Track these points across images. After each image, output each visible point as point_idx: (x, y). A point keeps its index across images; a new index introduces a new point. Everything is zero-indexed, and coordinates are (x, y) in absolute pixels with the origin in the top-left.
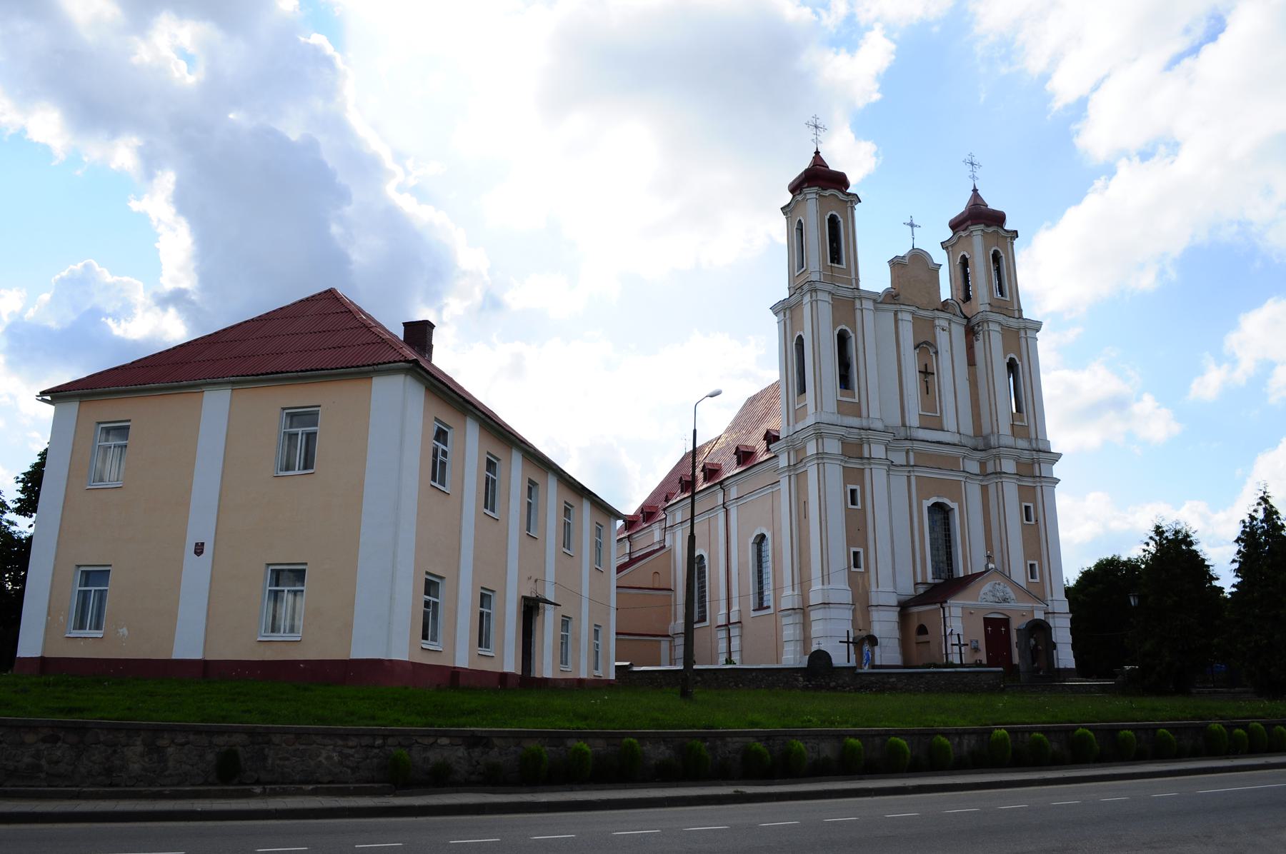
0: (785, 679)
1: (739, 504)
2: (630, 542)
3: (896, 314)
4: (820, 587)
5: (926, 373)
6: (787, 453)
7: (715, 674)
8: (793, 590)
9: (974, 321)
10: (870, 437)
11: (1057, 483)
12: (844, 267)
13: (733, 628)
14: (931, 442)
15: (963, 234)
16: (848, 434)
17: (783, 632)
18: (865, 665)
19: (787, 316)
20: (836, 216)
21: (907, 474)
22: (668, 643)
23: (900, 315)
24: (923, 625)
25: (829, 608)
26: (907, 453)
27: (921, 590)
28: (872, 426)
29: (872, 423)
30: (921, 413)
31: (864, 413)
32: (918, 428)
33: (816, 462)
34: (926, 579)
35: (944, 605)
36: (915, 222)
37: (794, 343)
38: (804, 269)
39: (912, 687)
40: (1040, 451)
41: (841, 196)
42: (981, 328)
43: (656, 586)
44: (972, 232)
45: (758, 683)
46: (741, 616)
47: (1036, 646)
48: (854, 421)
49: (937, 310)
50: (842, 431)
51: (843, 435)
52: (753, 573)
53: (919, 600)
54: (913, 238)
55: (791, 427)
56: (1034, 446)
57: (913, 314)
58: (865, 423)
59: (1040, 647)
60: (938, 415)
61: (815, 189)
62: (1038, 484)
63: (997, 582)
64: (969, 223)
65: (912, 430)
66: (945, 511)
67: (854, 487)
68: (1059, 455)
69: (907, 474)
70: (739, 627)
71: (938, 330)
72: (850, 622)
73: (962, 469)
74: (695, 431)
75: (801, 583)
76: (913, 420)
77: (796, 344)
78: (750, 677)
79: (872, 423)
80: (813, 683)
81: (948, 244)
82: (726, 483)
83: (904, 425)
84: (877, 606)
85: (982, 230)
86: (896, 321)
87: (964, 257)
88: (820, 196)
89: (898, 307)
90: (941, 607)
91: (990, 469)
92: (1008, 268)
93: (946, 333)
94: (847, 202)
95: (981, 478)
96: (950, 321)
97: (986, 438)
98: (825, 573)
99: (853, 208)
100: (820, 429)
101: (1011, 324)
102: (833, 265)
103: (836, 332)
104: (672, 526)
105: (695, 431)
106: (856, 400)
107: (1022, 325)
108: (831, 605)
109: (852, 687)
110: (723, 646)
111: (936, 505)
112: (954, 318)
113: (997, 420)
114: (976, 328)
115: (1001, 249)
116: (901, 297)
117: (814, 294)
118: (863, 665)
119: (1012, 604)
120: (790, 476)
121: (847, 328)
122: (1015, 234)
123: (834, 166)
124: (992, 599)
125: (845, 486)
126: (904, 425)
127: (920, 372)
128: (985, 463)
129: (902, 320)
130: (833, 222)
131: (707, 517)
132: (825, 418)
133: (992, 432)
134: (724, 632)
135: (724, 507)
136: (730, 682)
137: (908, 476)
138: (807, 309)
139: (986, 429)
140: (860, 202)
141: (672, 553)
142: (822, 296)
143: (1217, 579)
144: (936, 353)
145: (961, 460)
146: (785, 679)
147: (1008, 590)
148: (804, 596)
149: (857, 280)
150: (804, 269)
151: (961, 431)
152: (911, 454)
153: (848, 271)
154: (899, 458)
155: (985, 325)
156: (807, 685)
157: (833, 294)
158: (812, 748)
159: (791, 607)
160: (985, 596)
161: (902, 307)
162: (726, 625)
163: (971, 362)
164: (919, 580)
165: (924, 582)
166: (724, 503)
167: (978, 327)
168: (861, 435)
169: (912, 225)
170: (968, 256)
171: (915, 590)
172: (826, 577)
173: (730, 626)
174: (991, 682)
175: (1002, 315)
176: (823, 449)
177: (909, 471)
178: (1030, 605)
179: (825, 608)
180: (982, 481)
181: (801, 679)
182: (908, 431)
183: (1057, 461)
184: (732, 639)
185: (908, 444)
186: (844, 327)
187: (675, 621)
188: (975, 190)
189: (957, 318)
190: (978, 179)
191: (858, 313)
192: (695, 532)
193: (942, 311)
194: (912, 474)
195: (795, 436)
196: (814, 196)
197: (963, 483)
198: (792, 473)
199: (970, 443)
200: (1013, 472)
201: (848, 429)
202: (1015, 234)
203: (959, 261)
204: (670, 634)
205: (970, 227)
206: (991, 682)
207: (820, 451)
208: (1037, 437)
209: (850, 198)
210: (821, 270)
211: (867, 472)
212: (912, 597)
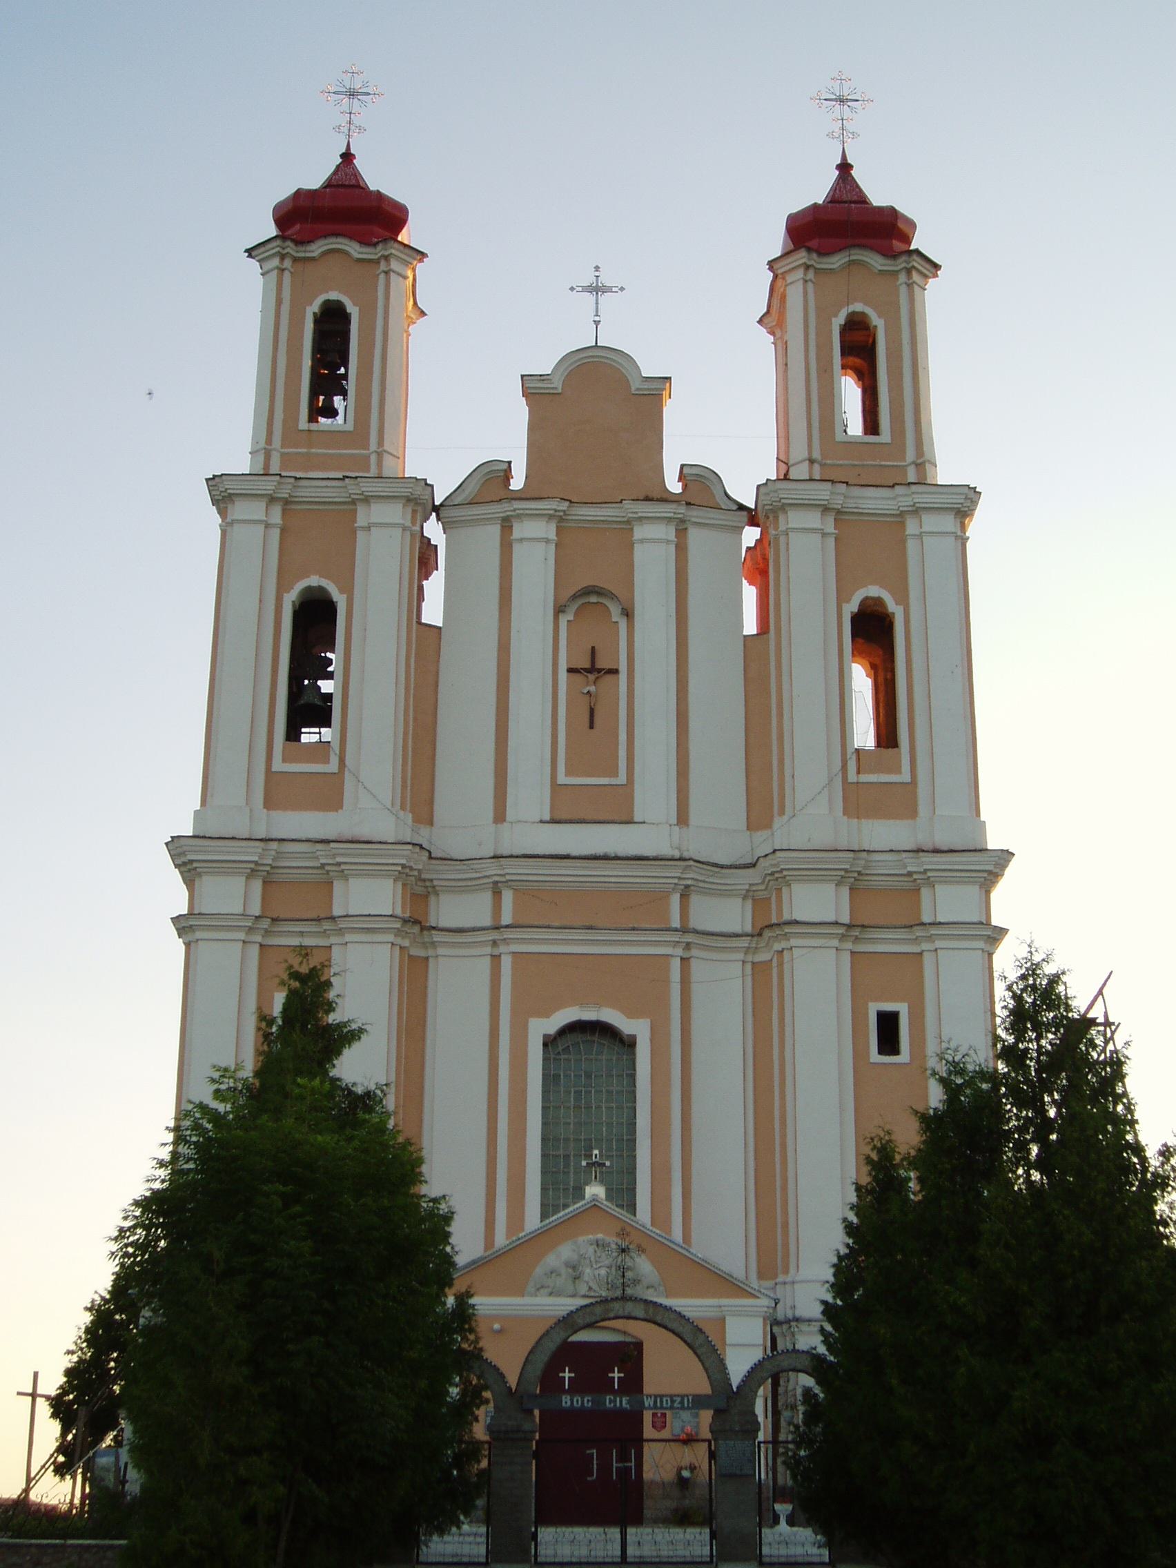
10: (339, 859)
14: (517, 857)
20: (863, 314)
21: (488, 950)
23: (519, 530)
26: (497, 894)
30: (562, 779)
36: (605, 280)
50: (251, 853)
54: (597, 323)
68: (1005, 857)
69: (488, 950)
88: (818, 271)
100: (334, 856)
103: (291, 598)
106: (905, 777)
115: (875, 309)
121: (325, 583)
123: (878, 196)
137: (682, 959)
143: (845, 1220)
144: (628, 614)
145: (675, 899)
152: (508, 897)
168: (317, 858)
177: (688, 946)
180: (747, 950)
188: (845, 168)
190: (831, 135)
191: (912, 545)
194: (502, 949)
197: (676, 964)
210: (816, 455)
211: (928, 959)
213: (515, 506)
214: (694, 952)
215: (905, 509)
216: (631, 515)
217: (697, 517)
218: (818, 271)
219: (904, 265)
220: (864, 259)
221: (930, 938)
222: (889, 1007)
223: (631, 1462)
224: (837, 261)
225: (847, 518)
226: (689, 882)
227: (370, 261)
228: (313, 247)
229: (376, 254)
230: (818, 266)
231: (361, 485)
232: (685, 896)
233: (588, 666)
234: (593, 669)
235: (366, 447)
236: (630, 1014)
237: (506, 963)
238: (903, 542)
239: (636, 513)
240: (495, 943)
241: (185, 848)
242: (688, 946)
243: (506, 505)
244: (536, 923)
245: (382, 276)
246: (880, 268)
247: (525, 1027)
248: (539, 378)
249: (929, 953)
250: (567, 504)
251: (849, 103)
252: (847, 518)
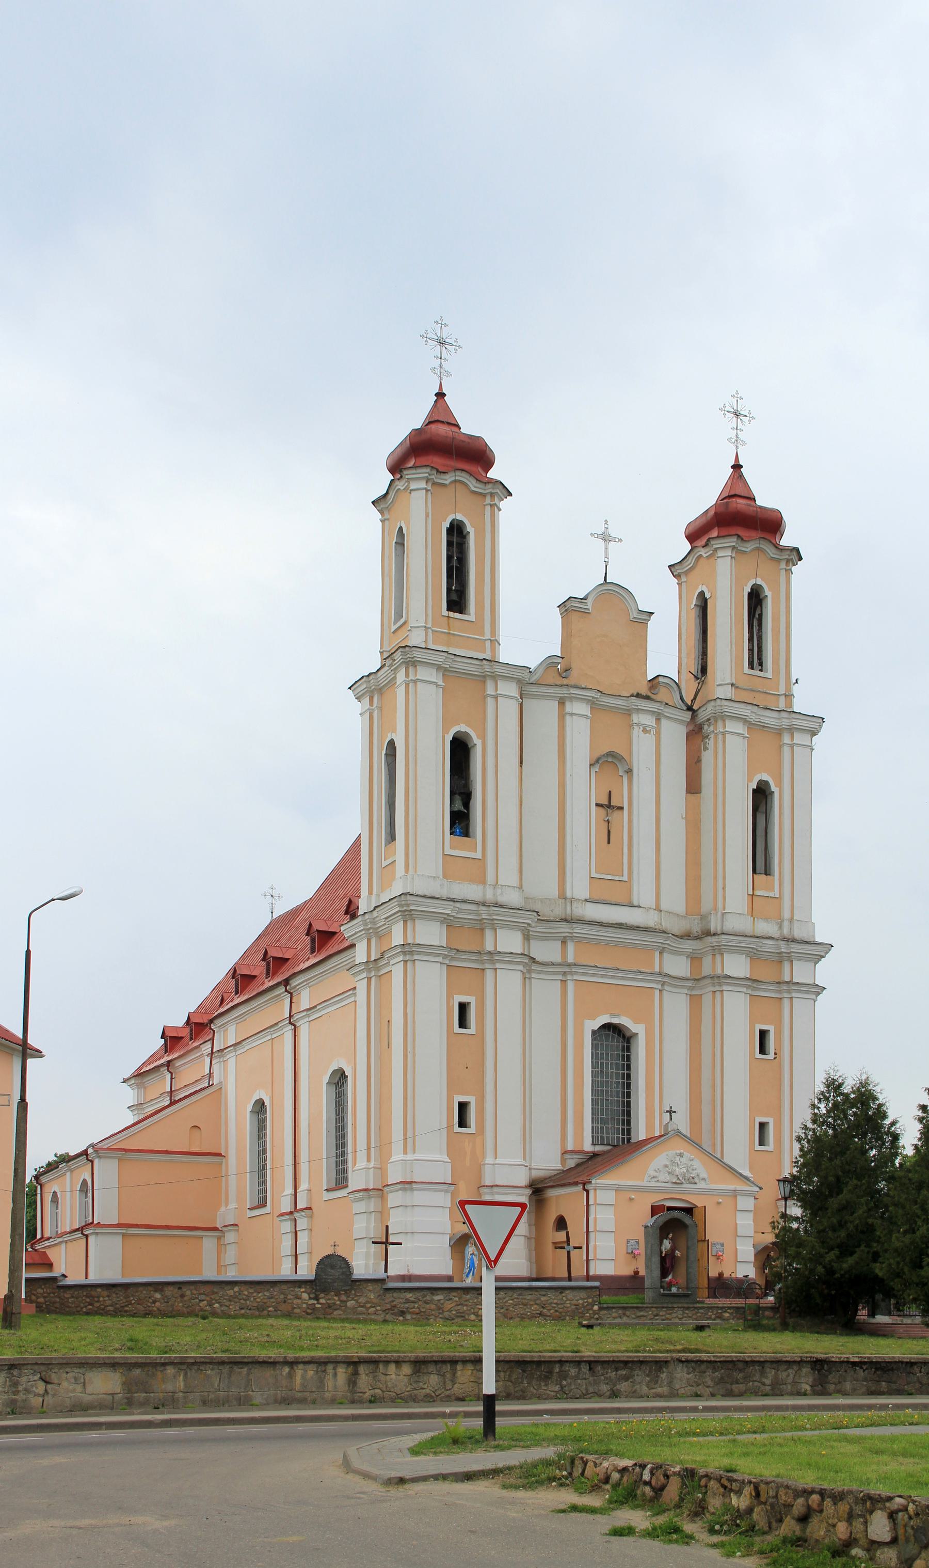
0: (282, 1296)
1: (311, 1018)
2: (172, 1074)
3: (562, 702)
4: (401, 1156)
5: (608, 806)
6: (366, 940)
7: (180, 1288)
8: (369, 1160)
9: (702, 716)
10: (495, 917)
11: (819, 994)
12: (472, 617)
13: (302, 1217)
15: (703, 552)
16: (458, 912)
17: (353, 1226)
18: (467, 1276)
19: (375, 704)
21: (561, 977)
22: (216, 1240)
23: (569, 707)
24: (563, 1216)
25: (412, 1189)
26: (564, 942)
27: (571, 1163)
28: (502, 899)
29: (502, 894)
30: (594, 875)
31: (490, 879)
32: (586, 900)
33: (401, 958)
34: (582, 1145)
35: (588, 1187)
36: (613, 532)
37: (384, 752)
38: (402, 621)
39: (465, 1308)
40: (794, 941)
41: (473, 484)
42: (712, 728)
43: (195, 1149)
44: (716, 549)
45: (242, 1301)
46: (310, 1199)
47: (673, 1249)
48: (471, 891)
49: (638, 696)
50: (447, 909)
51: (448, 915)
52: (328, 1131)
53: (562, 1179)
55: (373, 897)
56: (786, 931)
57: (593, 703)
58: (489, 896)
59: (678, 1253)
60: (625, 878)
61: (424, 472)
62: (785, 995)
63: (678, 1152)
64: (715, 533)
65: (574, 905)
66: (624, 1036)
67: (464, 999)
69: (561, 977)
70: (307, 1216)
71: (636, 732)
72: (448, 1210)
73: (657, 970)
74: (28, 953)
75: (380, 1147)
76: (579, 888)
77: (386, 755)
78: (231, 1293)
79: (502, 894)
80: (322, 1301)
81: (679, 570)
82: (294, 982)
83: (562, 896)
84: (492, 1186)
85: (734, 548)
86: (562, 717)
87: (702, 597)
89: (564, 692)
90: (584, 1189)
91: (707, 969)
92: (776, 619)
93: (650, 739)
94: (484, 495)
95: (689, 984)
96: (658, 717)
97: (704, 918)
98: (409, 1134)
99: (495, 507)
100: (408, 905)
101: (767, 720)
102: (451, 614)
103: (449, 737)
104: (222, 1050)
105: (28, 953)
107: (785, 723)
108: (414, 1186)
109: (378, 1308)
110: (287, 1242)
111: (607, 1027)
112: (668, 711)
113: (724, 888)
114: (706, 727)
116: (574, 673)
117: (411, 669)
118: (464, 1276)
119: (684, 1186)
120: (369, 979)
122: (795, 554)
124: (667, 1177)
125: (450, 997)
126: (562, 896)
127: (597, 805)
128: (700, 959)
129: (572, 714)
130: (457, 532)
131: (269, 1037)
132: (420, 888)
133: (715, 909)
134: (289, 1223)
135: (290, 1023)
136: (201, 1301)
138: (401, 692)
139: (706, 905)
140: (510, 494)
141: (223, 1096)
142: (424, 673)
144: (629, 771)
145: (657, 954)
146: (282, 1296)
147: (696, 1164)
148: (381, 1170)
149: (495, 642)
150: (402, 621)
151: (663, 907)
152: (571, 947)
153: (477, 625)
154: (544, 951)
155: (720, 723)
156: (314, 1304)
157: (446, 670)
158: (76, 1379)
159: (364, 1187)
160: (655, 1174)
161: (573, 691)
162: (291, 1213)
163: (693, 786)
164: (570, 1147)
165: (577, 1149)
166: (291, 1016)
167: (709, 726)
169: (606, 538)
170: (707, 595)
171: (563, 1161)
172: (410, 1141)
173: (296, 1215)
174: (581, 1302)
175: (750, 707)
176: (414, 937)
177: (564, 974)
178: (732, 1187)
179: (405, 1189)
181: (305, 1296)
182: (568, 908)
183: (822, 957)
184: (299, 1234)
185: (565, 928)
186: (463, 728)
187: (227, 1205)
189: (671, 710)
192: (27, 1098)
193: (647, 698)
195: (375, 914)
196: (423, 484)
198: (373, 974)
199: (677, 926)
200: (742, 975)
201: (458, 905)
202: (795, 554)
203: (694, 603)
204: (218, 1226)
205: (712, 542)
206: (581, 1302)
207: (410, 941)
208: (792, 918)
209: (489, 489)
212: (556, 1172)
213: (572, 692)
214: (666, 987)
215: (489, 674)
216: (633, 707)
217: (667, 712)
218: (434, 484)
219: (787, 557)
220: (765, 548)
221: (789, 991)
222: (765, 1027)
223: (27, 1280)
224: (749, 547)
225: (448, 674)
226: (666, 946)
227: (480, 494)
228: (446, 477)
229: (485, 490)
230: (435, 480)
231: (494, 667)
232: (661, 953)
233: (606, 802)
234: (609, 806)
235: (483, 634)
236: (637, 1021)
237: (570, 985)
238: (781, 746)
239: (637, 706)
240: (564, 974)
241: (409, 902)
242: (663, 984)
243: (565, 689)
244: (589, 964)
245: (488, 508)
246: (772, 556)
247: (583, 1024)
248: (580, 600)
249: (571, 982)
250: (600, 694)
251: (446, 346)
252: (448, 674)
